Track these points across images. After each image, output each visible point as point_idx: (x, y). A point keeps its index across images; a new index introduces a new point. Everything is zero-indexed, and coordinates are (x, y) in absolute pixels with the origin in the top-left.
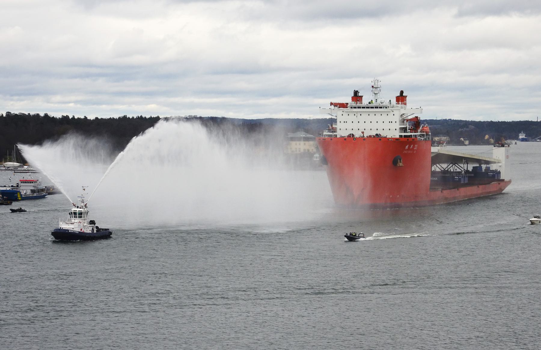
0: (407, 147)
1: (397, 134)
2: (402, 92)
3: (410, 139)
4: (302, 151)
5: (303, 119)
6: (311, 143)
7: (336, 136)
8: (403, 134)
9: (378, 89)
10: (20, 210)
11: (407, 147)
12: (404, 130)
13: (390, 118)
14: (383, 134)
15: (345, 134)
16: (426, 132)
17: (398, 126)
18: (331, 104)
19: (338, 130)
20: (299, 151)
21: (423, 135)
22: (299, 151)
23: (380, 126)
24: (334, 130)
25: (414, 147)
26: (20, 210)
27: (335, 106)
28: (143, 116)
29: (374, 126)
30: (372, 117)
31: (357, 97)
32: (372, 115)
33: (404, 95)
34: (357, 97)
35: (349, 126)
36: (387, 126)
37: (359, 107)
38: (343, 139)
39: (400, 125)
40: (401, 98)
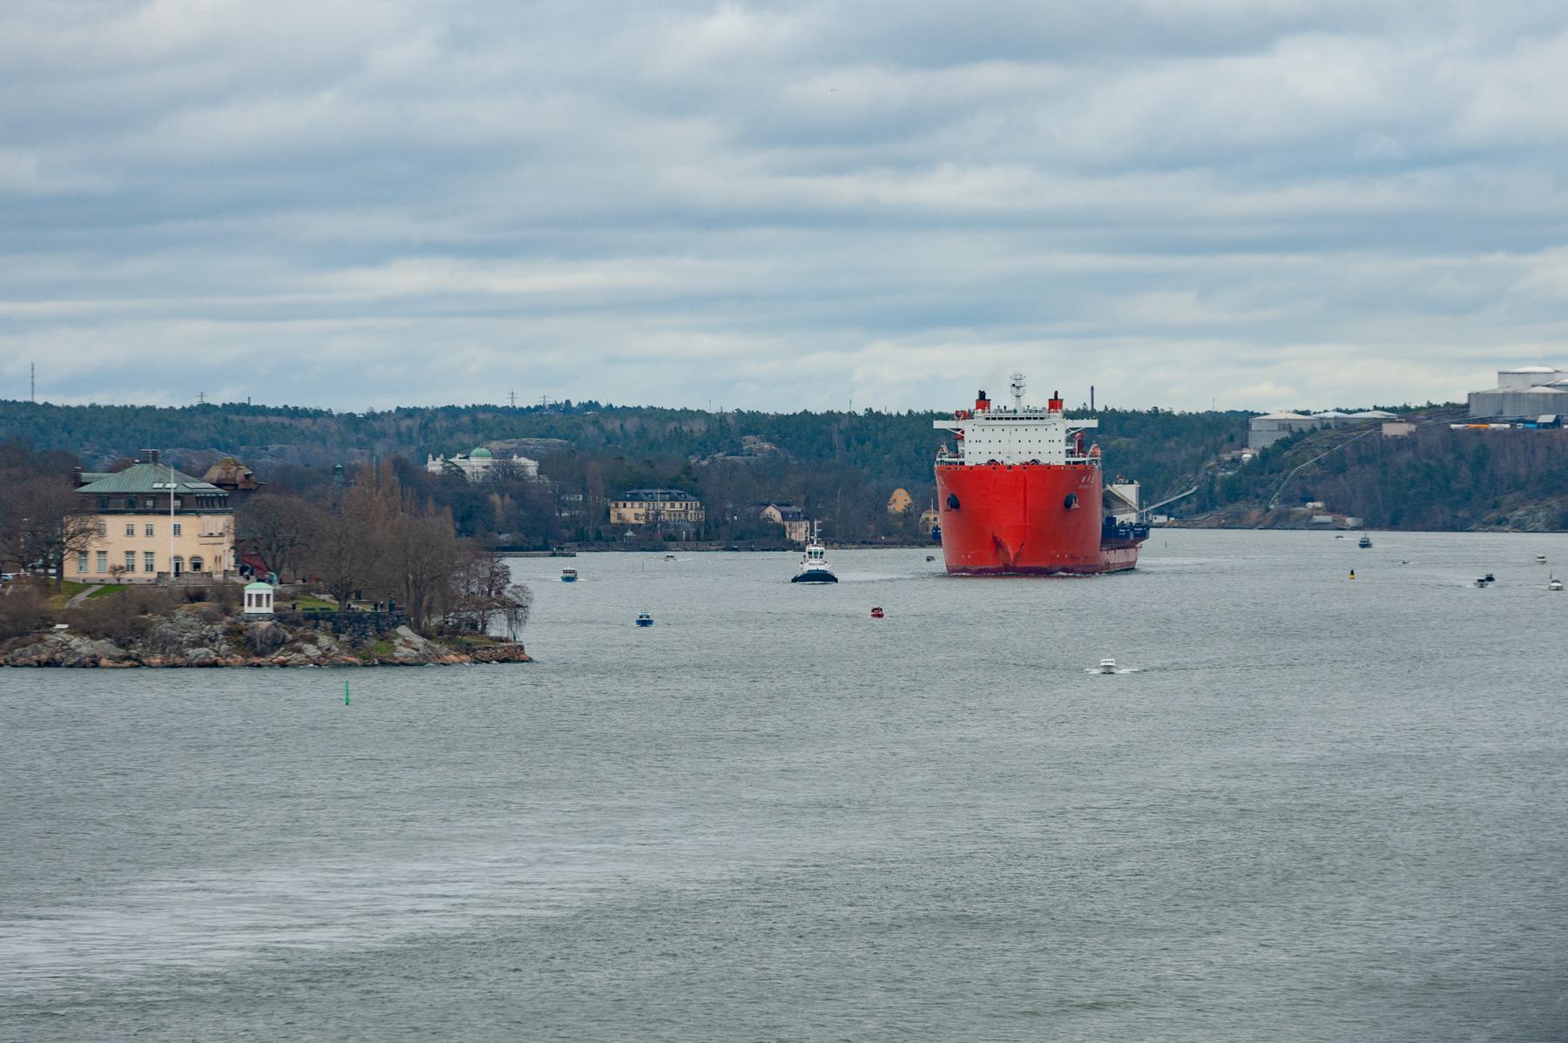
1: (1060, 460)
4: (163, 564)
5: (124, 409)
6: (219, 522)
7: (962, 463)
8: (1072, 460)
10: (825, 578)
12: (1070, 453)
13: (1051, 433)
14: (1044, 460)
15: (983, 460)
17: (1063, 447)
20: (150, 568)
22: (150, 568)
23: (995, 447)
24: (957, 454)
26: (825, 578)
28: (291, 406)
29: (1025, 447)
30: (1031, 434)
31: (983, 400)
32: (1021, 430)
34: (983, 400)
35: (985, 447)
36: (1045, 447)
38: (977, 471)
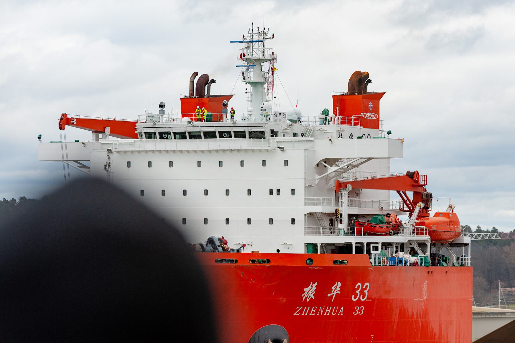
0: (310, 292)
1: (293, 241)
2: (360, 81)
3: (352, 260)
8: (320, 240)
9: (266, 66)
11: (310, 292)
13: (275, 175)
16: (431, 233)
17: (299, 208)
18: (65, 121)
19: (300, 219)
21: (422, 245)
25: (347, 291)
27: (96, 132)
33: (371, 88)
36: (261, 206)
37: (224, 135)
39: (306, 204)
40: (357, 103)
